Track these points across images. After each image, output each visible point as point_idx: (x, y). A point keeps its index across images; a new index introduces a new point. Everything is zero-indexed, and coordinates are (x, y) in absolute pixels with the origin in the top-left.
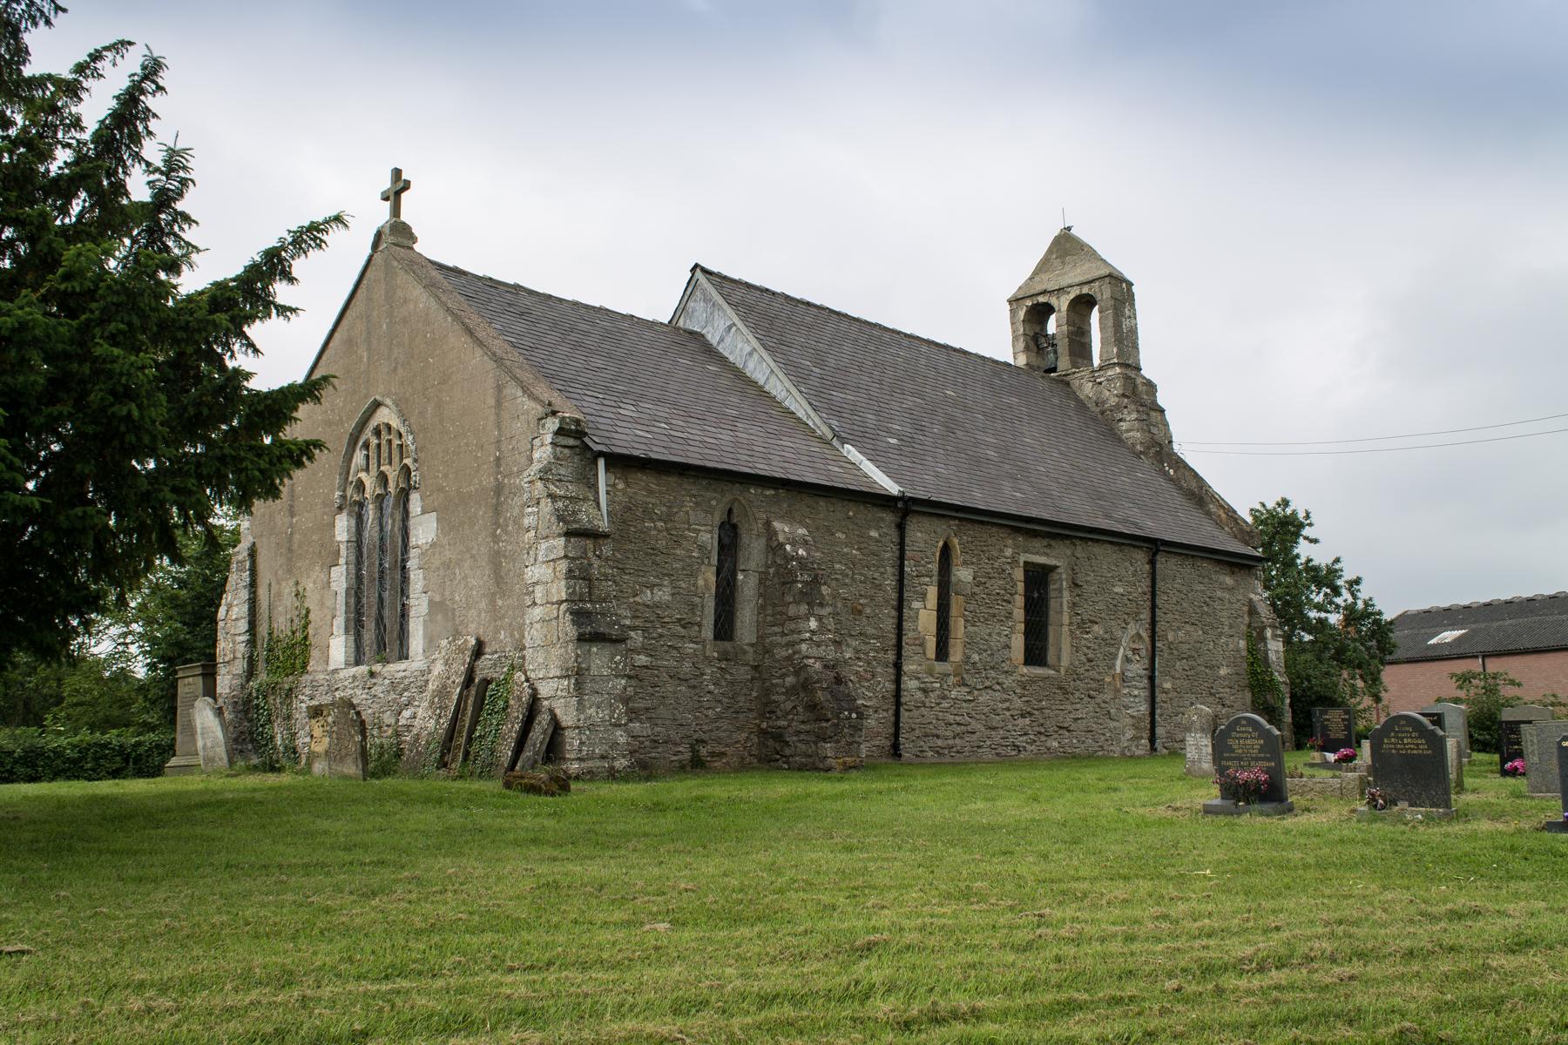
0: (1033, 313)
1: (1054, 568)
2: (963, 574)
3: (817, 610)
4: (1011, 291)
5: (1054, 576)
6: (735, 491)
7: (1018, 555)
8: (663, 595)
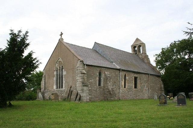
0: (134, 47)
1: (137, 77)
2: (127, 78)
3: (111, 82)
4: (131, 45)
5: (138, 78)
6: (101, 68)
7: (133, 76)
8: (93, 81)
